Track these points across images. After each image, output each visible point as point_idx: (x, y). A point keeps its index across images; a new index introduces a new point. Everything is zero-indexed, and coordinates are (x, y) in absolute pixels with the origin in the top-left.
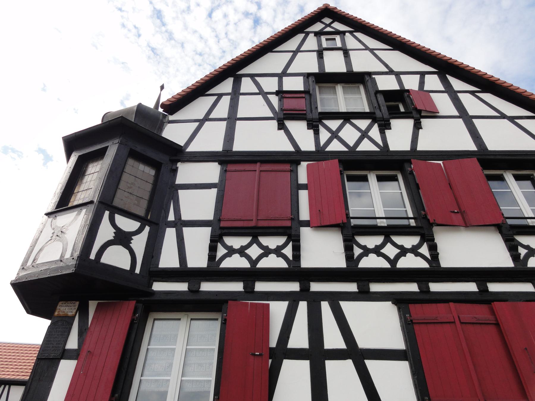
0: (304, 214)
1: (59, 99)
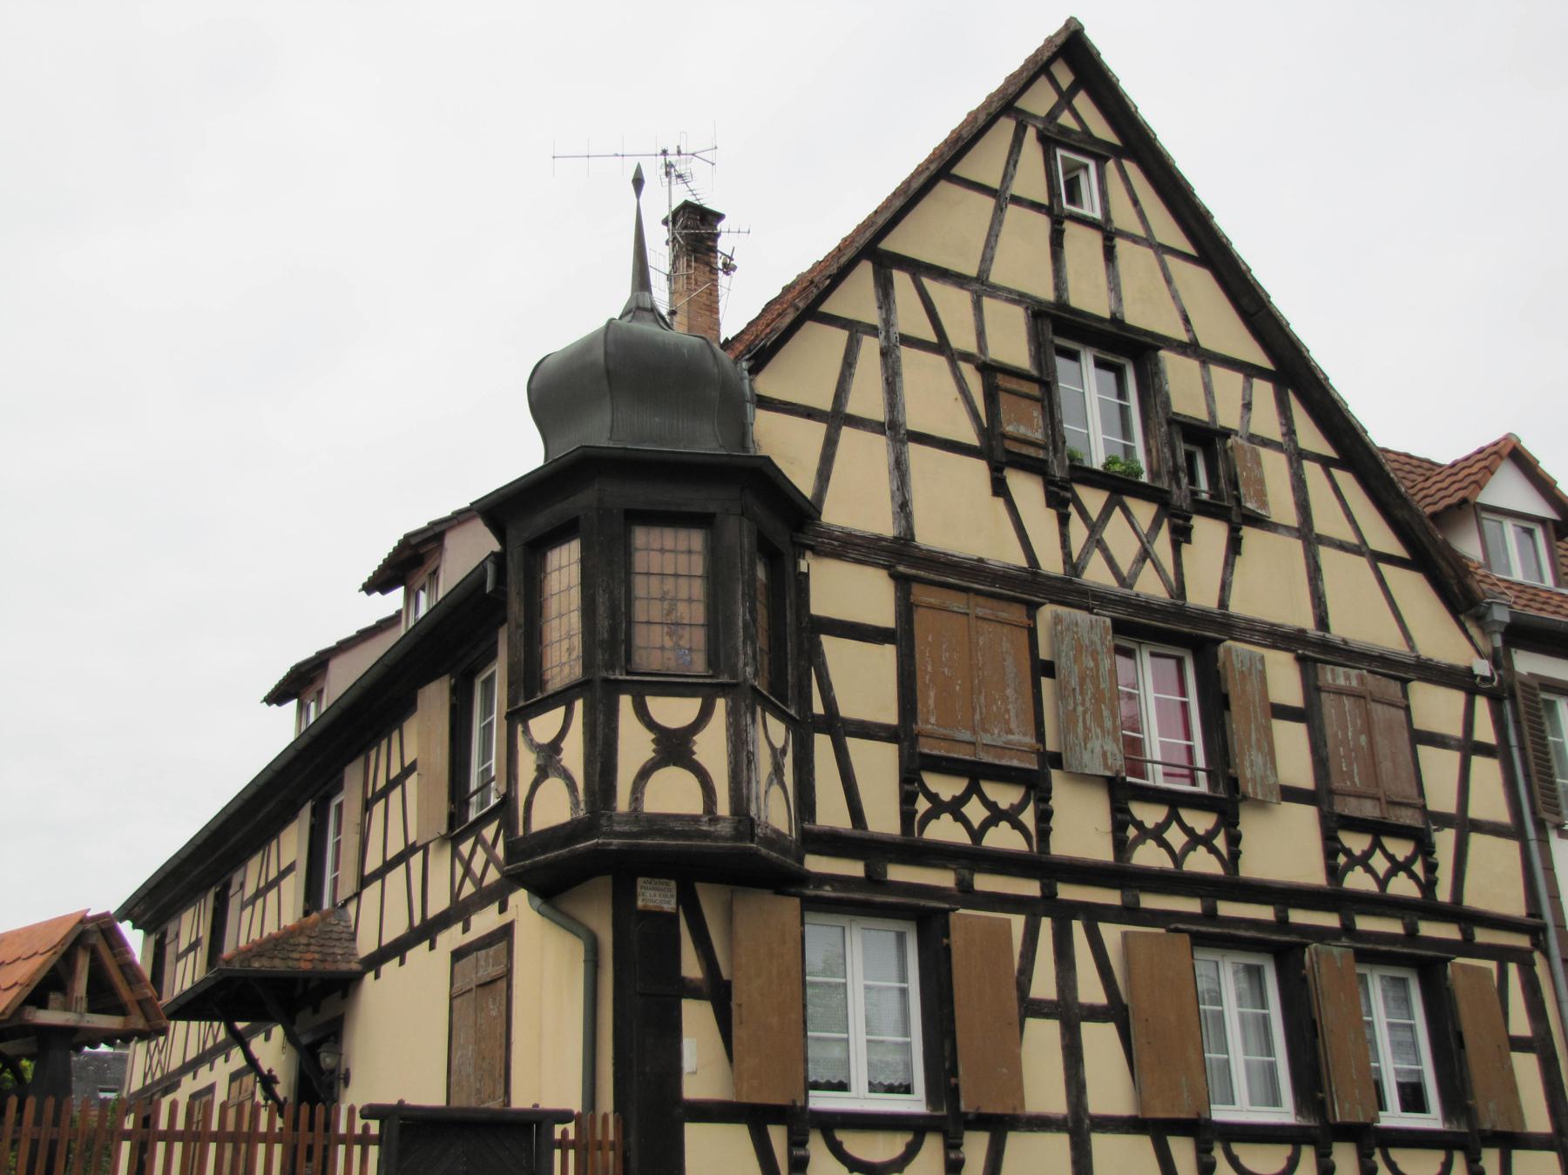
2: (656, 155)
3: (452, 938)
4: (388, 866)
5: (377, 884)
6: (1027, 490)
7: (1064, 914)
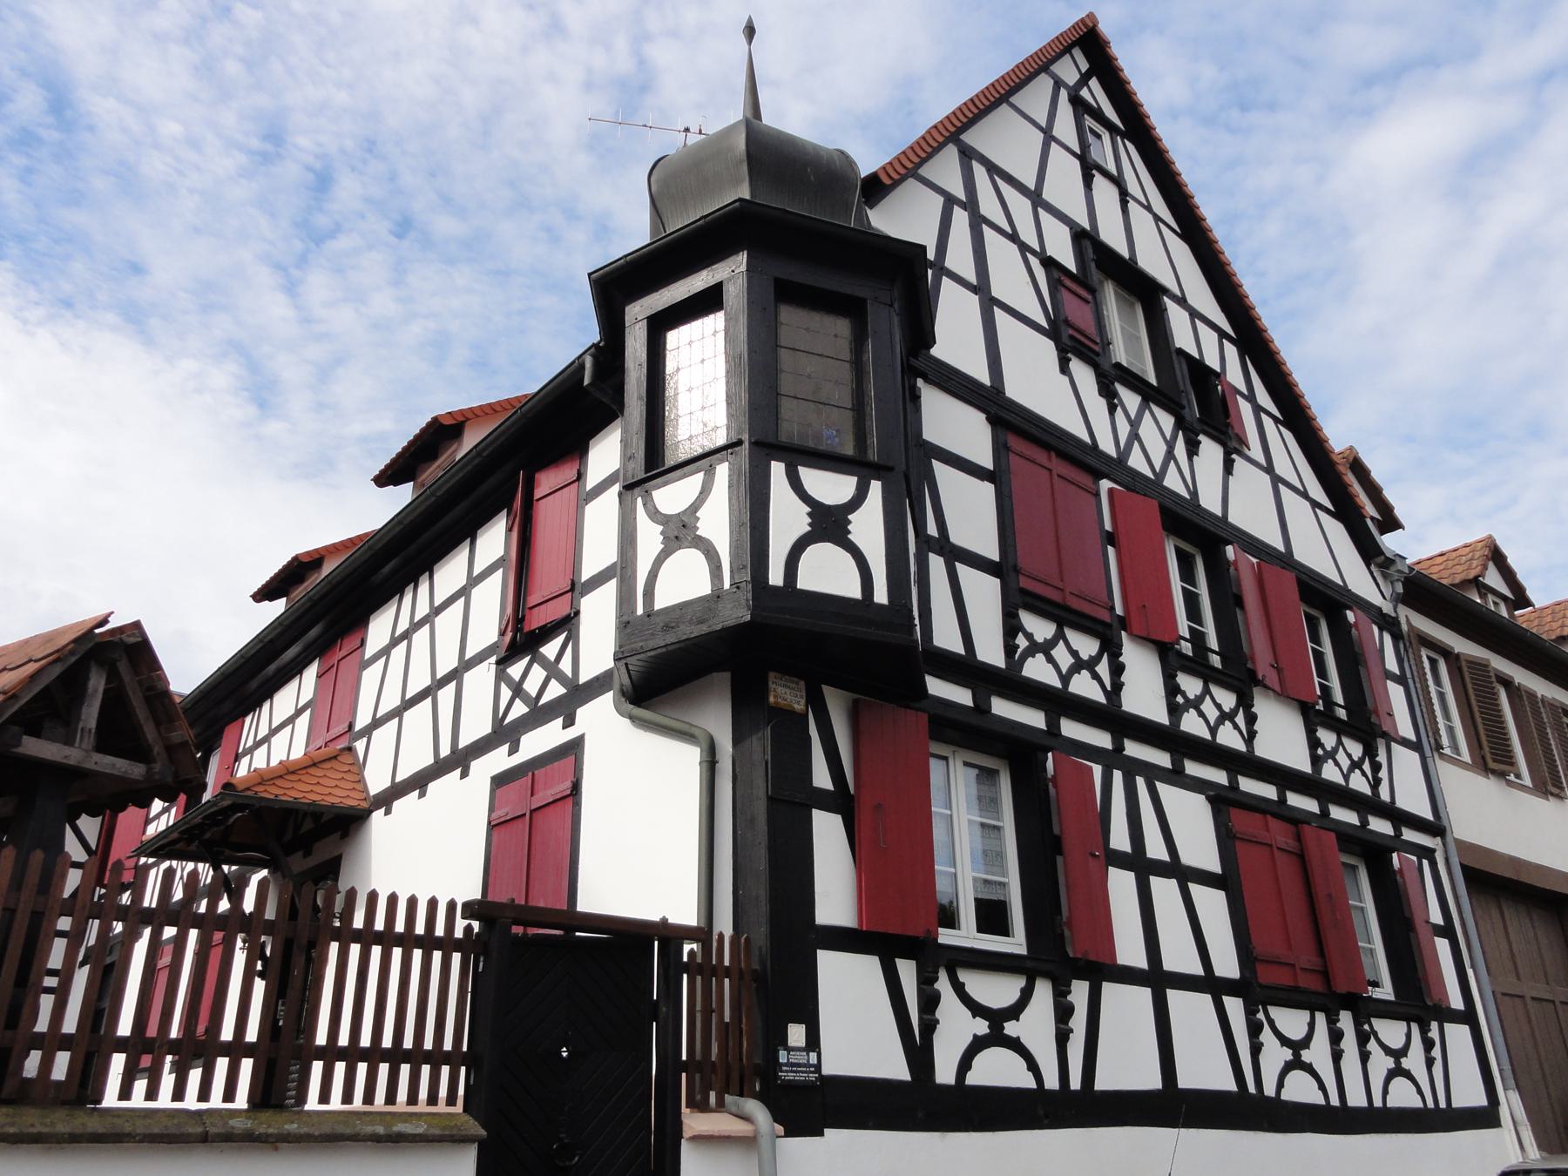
2: (680, 131)
3: (499, 760)
4: (408, 704)
5: (441, 673)
6: (1084, 374)
7: (1133, 768)
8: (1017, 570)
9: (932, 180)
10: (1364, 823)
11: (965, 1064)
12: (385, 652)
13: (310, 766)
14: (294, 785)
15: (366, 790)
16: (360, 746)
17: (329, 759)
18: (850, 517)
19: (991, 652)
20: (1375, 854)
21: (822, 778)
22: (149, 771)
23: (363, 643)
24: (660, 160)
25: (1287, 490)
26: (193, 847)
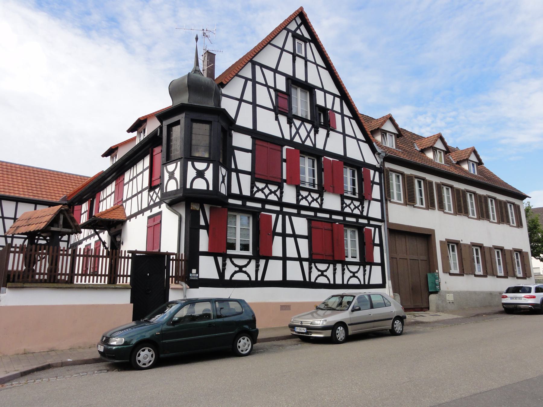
0: (285, 177)
1: (446, 282)
3: (148, 213)
6: (283, 119)
7: (284, 214)
8: (255, 174)
9: (241, 75)
10: (357, 221)
11: (359, 269)
12: (128, 183)
13: (113, 210)
14: (109, 215)
15: (126, 215)
16: (124, 204)
17: (117, 208)
18: (205, 172)
19: (246, 192)
20: (360, 228)
21: (202, 223)
22: (72, 230)
23: (124, 179)
24: (172, 81)
25: (352, 136)
26: (90, 226)
